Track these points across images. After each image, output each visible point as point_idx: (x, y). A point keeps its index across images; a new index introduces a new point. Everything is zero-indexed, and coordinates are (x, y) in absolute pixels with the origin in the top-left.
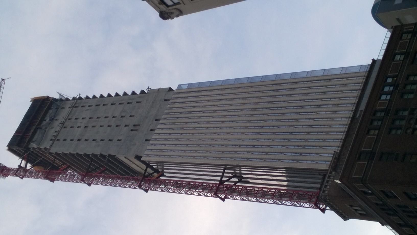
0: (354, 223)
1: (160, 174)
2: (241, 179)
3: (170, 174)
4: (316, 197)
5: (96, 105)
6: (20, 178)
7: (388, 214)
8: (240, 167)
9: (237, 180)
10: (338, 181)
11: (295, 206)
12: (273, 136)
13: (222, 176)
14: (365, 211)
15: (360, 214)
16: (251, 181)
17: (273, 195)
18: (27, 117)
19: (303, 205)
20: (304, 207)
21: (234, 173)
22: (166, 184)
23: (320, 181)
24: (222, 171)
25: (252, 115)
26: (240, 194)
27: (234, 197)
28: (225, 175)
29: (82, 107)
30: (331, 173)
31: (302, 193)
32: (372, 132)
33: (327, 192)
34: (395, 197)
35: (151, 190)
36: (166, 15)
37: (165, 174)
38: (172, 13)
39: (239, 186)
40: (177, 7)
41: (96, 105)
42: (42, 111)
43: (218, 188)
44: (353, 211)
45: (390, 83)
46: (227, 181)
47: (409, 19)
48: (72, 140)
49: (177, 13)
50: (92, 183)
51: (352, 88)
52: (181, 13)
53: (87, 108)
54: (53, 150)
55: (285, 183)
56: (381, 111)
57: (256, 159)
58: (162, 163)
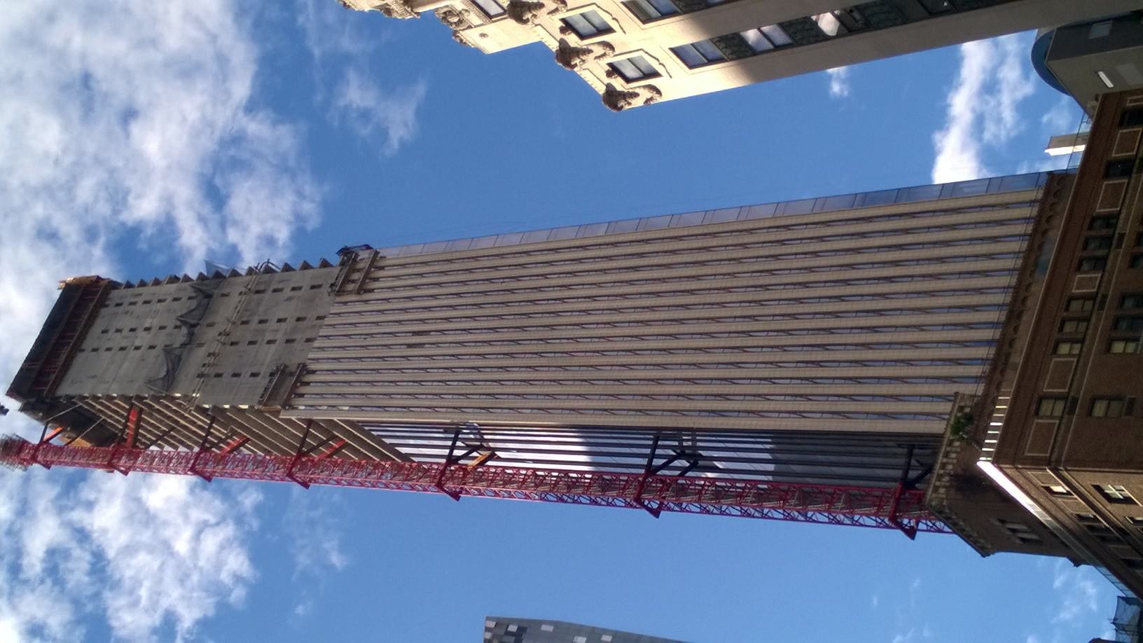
3: (725, 466)
5: (313, 287)
6: (651, 510)
8: (693, 431)
13: (653, 456)
14: (1036, 533)
15: (1023, 540)
16: (719, 465)
17: (740, 495)
18: (51, 326)
19: (861, 521)
20: (861, 525)
21: (681, 446)
22: (720, 494)
23: (902, 461)
27: (766, 511)
28: (658, 452)
29: (275, 291)
31: (856, 492)
32: (1064, 349)
37: (499, 454)
41: (313, 287)
44: (1008, 533)
45: (953, 189)
47: (1133, 76)
48: (254, 375)
50: (52, 462)
53: (288, 293)
55: (771, 467)
56: (1084, 298)
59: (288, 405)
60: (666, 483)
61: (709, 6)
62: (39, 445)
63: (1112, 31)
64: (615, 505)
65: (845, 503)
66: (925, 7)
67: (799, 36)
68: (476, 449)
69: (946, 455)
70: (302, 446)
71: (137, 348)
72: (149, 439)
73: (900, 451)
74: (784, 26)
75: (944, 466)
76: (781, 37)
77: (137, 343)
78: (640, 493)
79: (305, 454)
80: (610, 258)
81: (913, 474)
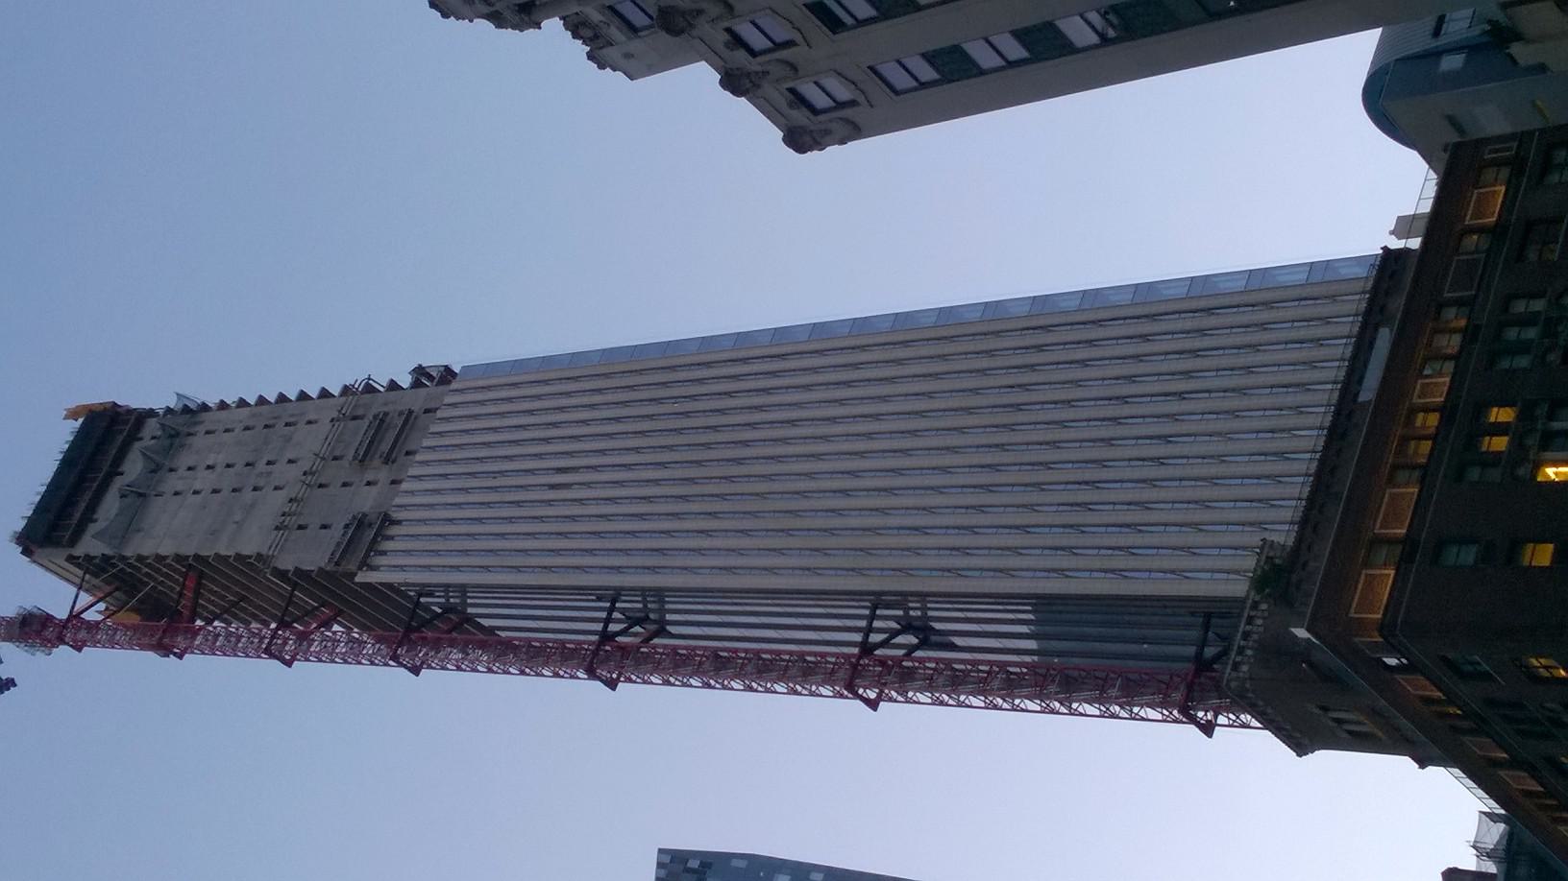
0: (1328, 761)
1: (653, 627)
2: (927, 636)
3: (686, 629)
4: (1182, 687)
7: (1454, 729)
8: (923, 596)
9: (915, 641)
10: (1301, 633)
11: (942, 703)
13: (869, 630)
15: (1350, 733)
16: (959, 641)
18: (68, 462)
19: (1142, 713)
24: (867, 612)
26: (930, 685)
28: (877, 624)
30: (1255, 606)
33: (1245, 668)
34: (1486, 676)
35: (430, 667)
37: (669, 628)
38: (827, 132)
39: (922, 660)
40: (848, 113)
42: (107, 446)
43: (855, 667)
46: (884, 644)
50: (84, 644)
54: (286, 563)
55: (1032, 644)
58: (660, 593)
59: (365, 564)
60: (623, 649)
61: (919, 8)
62: (68, 620)
63: (1467, 62)
65: (1060, 684)
66: (1204, 8)
68: (638, 622)
69: (1250, 620)
70: (412, 619)
71: (196, 492)
72: (212, 612)
73: (1189, 619)
75: (1246, 635)
76: (1015, 51)
77: (198, 487)
79: (418, 630)
80: (814, 370)
81: (1210, 652)
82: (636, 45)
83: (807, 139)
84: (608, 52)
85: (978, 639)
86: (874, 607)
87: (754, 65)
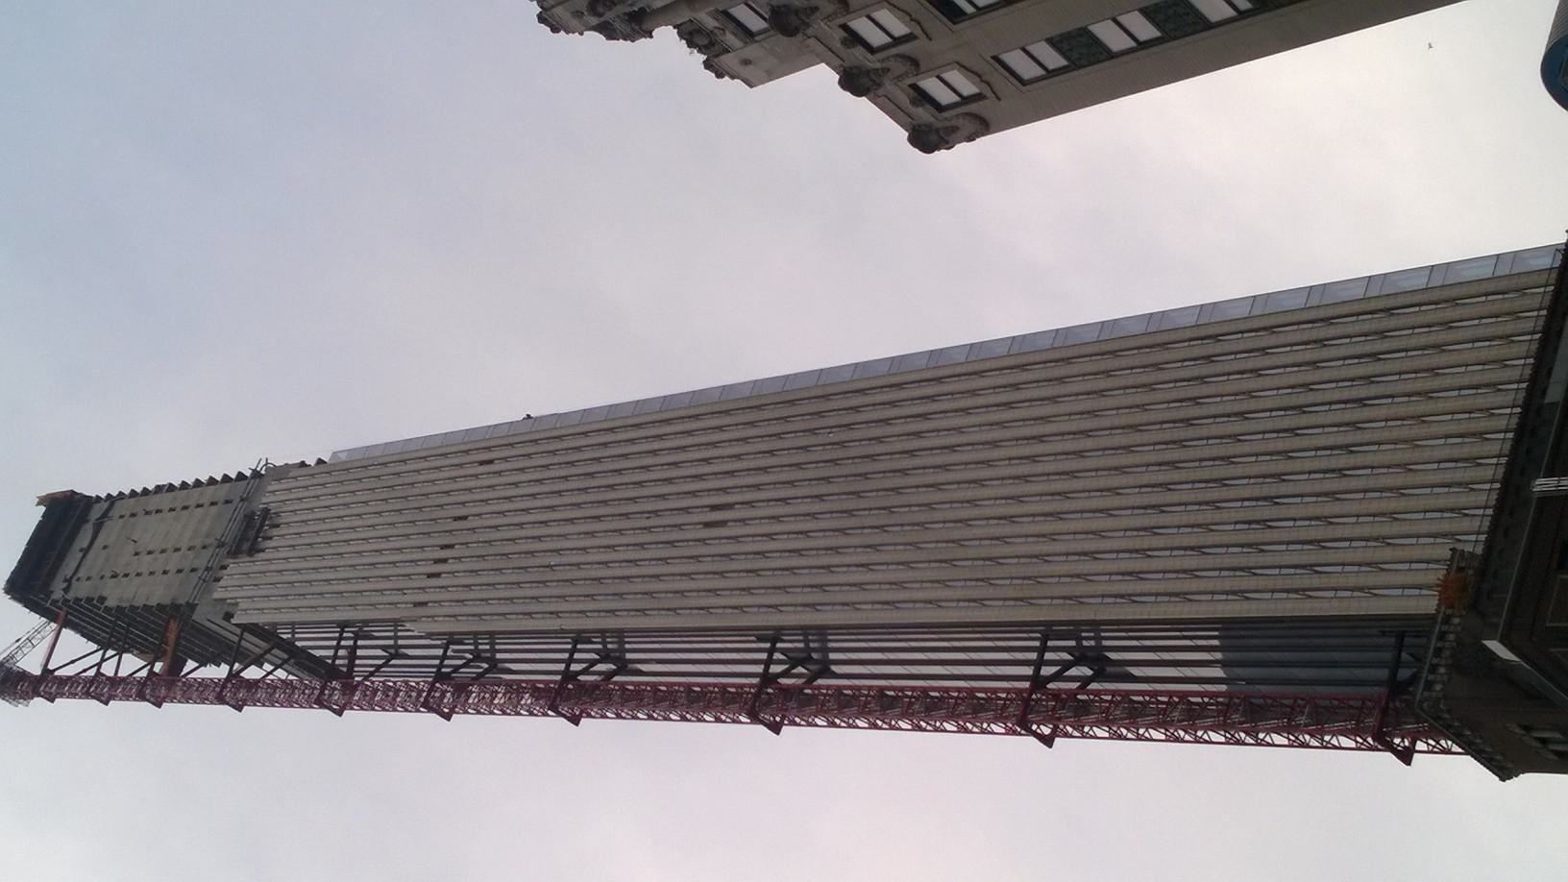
0: (1531, 784)
2: (1103, 668)
3: (852, 668)
4: (1376, 712)
6: (1042, 738)
8: (1095, 625)
9: (1089, 672)
12: (1208, 516)
13: (1039, 663)
15: (1557, 753)
16: (1136, 671)
19: (1334, 741)
20: (1335, 747)
21: (1079, 646)
22: (515, 690)
24: (1037, 644)
25: (1128, 449)
28: (1048, 656)
30: (1447, 620)
31: (1326, 703)
33: (1438, 687)
36: (934, 138)
37: (834, 668)
38: (954, 129)
40: (973, 108)
42: (66, 518)
43: (1027, 701)
44: (1534, 743)
49: (970, 126)
51: (1469, 334)
52: (984, 127)
57: (1157, 595)
58: (822, 631)
64: (993, 733)
65: (1310, 716)
67: (1075, 55)
73: (1382, 640)
74: (1054, 43)
75: (1438, 652)
78: (1025, 714)
81: (1404, 674)
82: (752, 51)
83: (934, 138)
84: (727, 60)
85: (1154, 671)
86: (576, 642)
87: (872, 62)
